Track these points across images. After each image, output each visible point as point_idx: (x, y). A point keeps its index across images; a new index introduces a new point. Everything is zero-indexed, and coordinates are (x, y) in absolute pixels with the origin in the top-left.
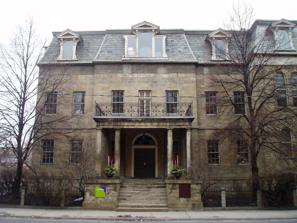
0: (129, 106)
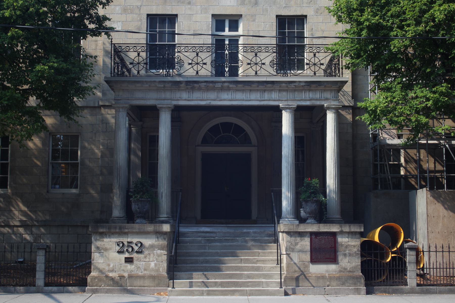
0: (205, 51)
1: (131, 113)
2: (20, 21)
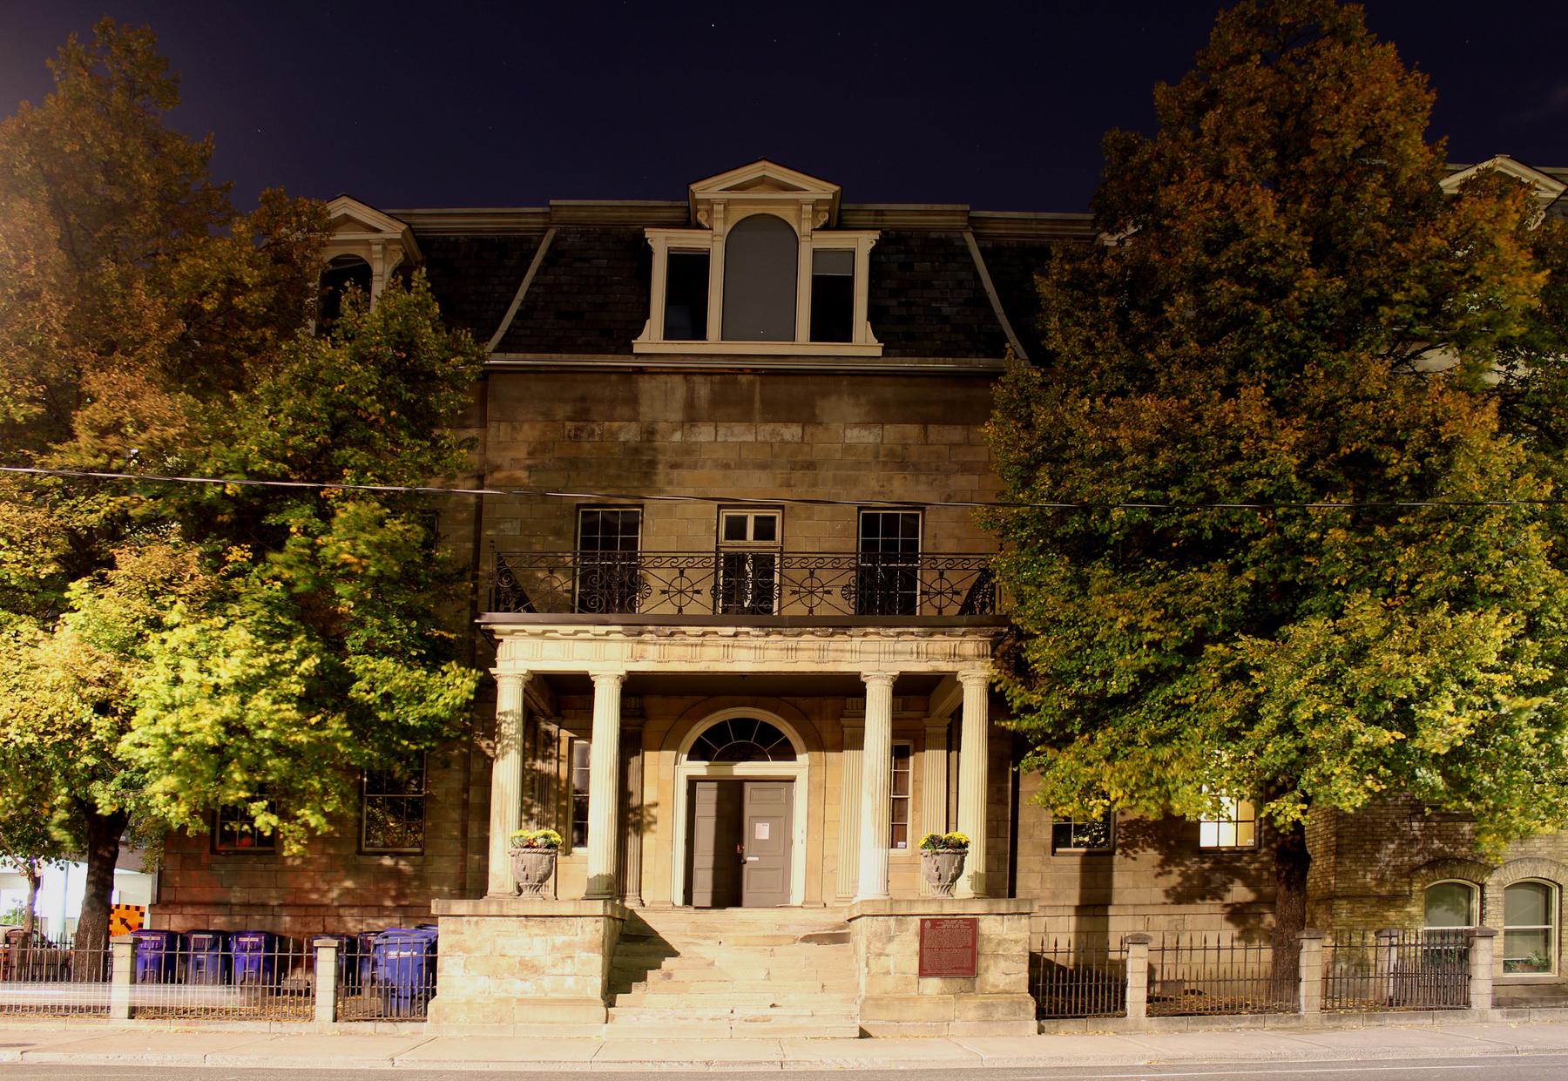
1: (531, 689)
2: (1405, 509)
